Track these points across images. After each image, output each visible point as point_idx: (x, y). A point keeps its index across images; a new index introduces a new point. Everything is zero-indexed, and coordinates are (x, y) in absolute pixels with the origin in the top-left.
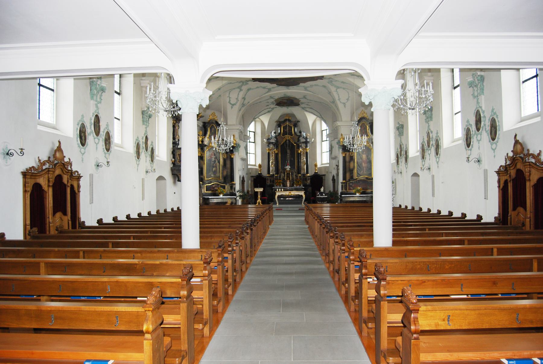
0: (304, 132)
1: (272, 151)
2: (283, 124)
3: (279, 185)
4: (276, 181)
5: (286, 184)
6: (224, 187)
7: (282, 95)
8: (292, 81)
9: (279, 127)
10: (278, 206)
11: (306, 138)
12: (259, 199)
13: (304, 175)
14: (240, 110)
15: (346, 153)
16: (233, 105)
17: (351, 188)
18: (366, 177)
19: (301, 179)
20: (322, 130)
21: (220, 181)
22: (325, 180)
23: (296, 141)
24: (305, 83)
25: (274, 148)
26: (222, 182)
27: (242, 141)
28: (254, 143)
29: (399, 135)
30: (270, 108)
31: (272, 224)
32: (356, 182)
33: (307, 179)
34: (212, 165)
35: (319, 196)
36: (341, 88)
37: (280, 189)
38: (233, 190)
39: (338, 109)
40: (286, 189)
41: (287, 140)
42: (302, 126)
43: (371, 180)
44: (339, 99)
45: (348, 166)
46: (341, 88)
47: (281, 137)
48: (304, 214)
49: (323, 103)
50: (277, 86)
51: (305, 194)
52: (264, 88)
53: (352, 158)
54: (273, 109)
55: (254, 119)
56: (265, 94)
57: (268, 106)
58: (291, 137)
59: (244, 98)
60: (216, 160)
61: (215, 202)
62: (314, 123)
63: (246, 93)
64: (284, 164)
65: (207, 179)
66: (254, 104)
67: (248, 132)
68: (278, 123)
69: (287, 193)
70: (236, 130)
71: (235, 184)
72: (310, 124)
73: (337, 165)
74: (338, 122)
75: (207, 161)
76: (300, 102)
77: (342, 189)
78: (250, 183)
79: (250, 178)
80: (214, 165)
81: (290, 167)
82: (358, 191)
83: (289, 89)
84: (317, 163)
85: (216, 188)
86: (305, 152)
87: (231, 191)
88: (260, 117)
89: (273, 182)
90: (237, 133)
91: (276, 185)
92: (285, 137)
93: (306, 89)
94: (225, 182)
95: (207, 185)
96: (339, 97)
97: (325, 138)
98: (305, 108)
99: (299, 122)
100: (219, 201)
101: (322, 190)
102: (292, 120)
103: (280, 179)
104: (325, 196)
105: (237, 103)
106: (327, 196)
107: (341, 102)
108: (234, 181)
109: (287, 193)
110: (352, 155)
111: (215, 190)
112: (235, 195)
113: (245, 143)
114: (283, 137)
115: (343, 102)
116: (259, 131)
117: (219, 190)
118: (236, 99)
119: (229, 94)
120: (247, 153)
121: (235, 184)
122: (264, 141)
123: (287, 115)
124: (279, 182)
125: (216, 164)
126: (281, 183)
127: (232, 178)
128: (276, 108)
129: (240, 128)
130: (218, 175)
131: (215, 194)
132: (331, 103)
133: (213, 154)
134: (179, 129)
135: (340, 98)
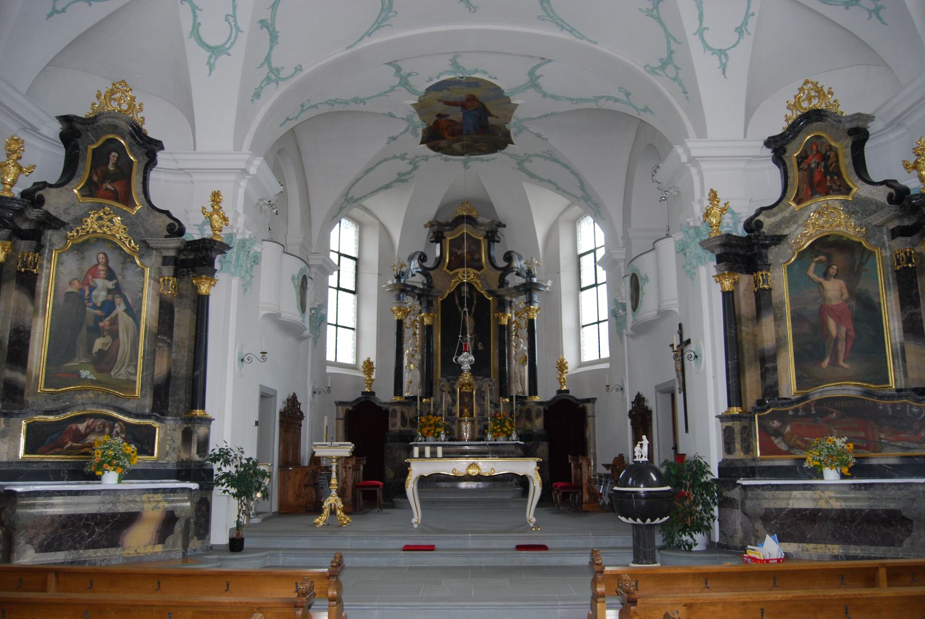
1: (413, 318)
5: (460, 431)
9: (437, 242)
11: (530, 274)
12: (334, 492)
13: (521, 399)
14: (257, 95)
16: (216, 51)
19: (511, 413)
20: (580, 251)
23: (494, 287)
25: (418, 308)
30: (403, 157)
33: (534, 413)
34: (90, 321)
37: (428, 450)
40: (460, 448)
42: (510, 240)
44: (700, 33)
47: (445, 272)
49: (609, 98)
51: (539, 471)
61: (54, 518)
62: (552, 233)
64: (452, 346)
69: (460, 466)
70: (233, 177)
71: (208, 421)
72: (540, 233)
75: (61, 300)
76: (513, 120)
77: (728, 446)
78: (326, 424)
80: (105, 323)
81: (472, 358)
82: (836, 459)
86: (524, 323)
87: (184, 456)
89: (414, 423)
94: (160, 409)
99: (504, 226)
100: (88, 506)
102: (480, 220)
103: (439, 412)
104: (661, 482)
106: (668, 488)
107: (707, 47)
108: (203, 407)
109: (460, 466)
115: (717, 47)
116: (372, 256)
121: (208, 421)
123: (465, 202)
124: (432, 422)
125: (115, 321)
126: (440, 427)
128: (427, 158)
132: (649, 76)
133: (102, 273)
135: (704, 25)
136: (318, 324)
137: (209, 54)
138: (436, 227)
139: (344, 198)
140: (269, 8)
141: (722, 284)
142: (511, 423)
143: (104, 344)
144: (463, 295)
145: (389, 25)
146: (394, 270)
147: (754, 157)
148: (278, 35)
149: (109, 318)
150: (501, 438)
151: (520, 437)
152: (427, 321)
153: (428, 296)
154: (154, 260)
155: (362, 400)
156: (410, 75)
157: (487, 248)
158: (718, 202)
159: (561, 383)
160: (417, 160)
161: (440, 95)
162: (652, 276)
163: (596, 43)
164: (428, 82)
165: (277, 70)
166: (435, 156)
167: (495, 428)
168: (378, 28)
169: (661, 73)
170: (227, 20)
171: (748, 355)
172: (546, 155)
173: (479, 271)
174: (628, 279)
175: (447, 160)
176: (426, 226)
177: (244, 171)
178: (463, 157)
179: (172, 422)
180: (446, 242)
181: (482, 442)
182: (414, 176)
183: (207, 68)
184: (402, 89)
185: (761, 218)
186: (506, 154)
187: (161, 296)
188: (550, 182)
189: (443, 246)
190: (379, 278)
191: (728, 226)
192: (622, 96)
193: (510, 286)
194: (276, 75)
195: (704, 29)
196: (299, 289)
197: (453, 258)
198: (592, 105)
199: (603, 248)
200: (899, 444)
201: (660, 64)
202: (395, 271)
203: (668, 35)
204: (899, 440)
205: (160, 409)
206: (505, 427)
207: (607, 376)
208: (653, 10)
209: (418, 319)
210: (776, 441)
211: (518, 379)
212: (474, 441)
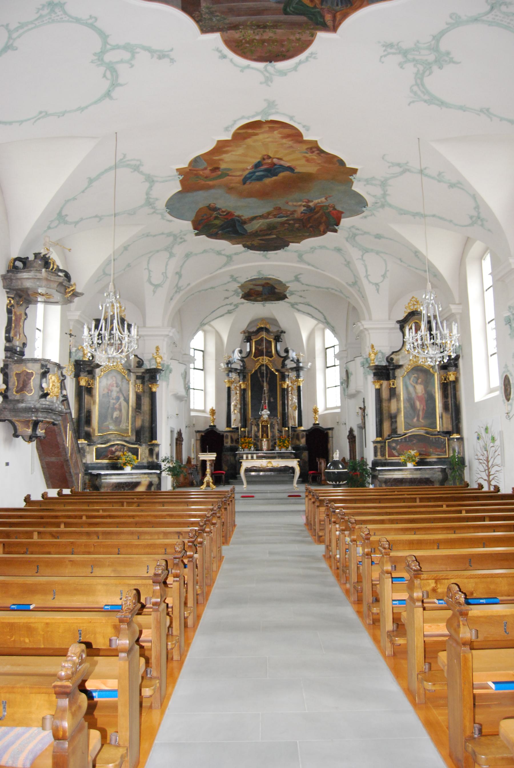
0: (293, 351)
1: (235, 385)
2: (254, 337)
3: (248, 448)
4: (243, 440)
6: (135, 452)
7: (253, 275)
8: (274, 236)
9: (247, 342)
10: (245, 489)
11: (298, 361)
13: (294, 429)
14: (171, 299)
15: (382, 381)
16: (157, 286)
17: (394, 452)
18: (426, 430)
19: (289, 436)
20: (326, 347)
21: (127, 439)
22: (332, 437)
23: (279, 367)
25: (238, 379)
26: (133, 442)
27: (177, 362)
28: (202, 370)
29: (510, 334)
30: (231, 304)
31: (233, 539)
32: (403, 440)
33: (300, 436)
34: (111, 406)
35: (330, 469)
36: (372, 250)
37: (250, 456)
38: (155, 457)
39: (363, 297)
41: (263, 365)
42: (288, 340)
43: (435, 435)
44: (367, 276)
45: (387, 408)
46: (372, 250)
47: (252, 359)
48: (303, 507)
49: (332, 289)
52: (219, 253)
53: (393, 393)
54: (237, 306)
55: (201, 326)
56: (220, 268)
57: (228, 298)
58: (270, 359)
59: (179, 274)
60: (121, 396)
62: (311, 336)
63: (183, 264)
64: (257, 407)
65: (99, 434)
66: (200, 291)
67: (192, 351)
68: (247, 334)
71: (158, 445)
72: (305, 336)
73: (360, 408)
74: (363, 322)
76: (288, 291)
77: (376, 455)
79: (195, 433)
81: (269, 412)
82: (411, 459)
83: (268, 259)
84: (318, 407)
85: (117, 453)
86: (295, 387)
87: (150, 460)
88: (212, 323)
89: (237, 441)
90: (165, 343)
91: (242, 448)
92: (259, 359)
93: (300, 257)
94: (138, 440)
95: (99, 446)
96: (367, 271)
97: (331, 361)
98: (296, 304)
99: (285, 332)
101: (336, 456)
102: (271, 330)
103: (250, 436)
106: (346, 470)
107: (370, 282)
108: (156, 439)
109: (264, 463)
110: (394, 387)
111: (117, 456)
112: (157, 467)
113: (182, 368)
114: (256, 359)
116: (212, 349)
117: (124, 458)
118: (163, 274)
119: (148, 263)
120: (187, 389)
122: (221, 367)
123: (262, 320)
125: (120, 405)
127: (153, 435)
128: (243, 303)
129: (171, 334)
130: (123, 426)
131: (115, 466)
133: (115, 385)
134: (26, 321)
135: (368, 273)
141: (375, 385)
142: (288, 441)
143: (117, 415)
144: (262, 371)
149: (118, 403)
150: (283, 449)
151: (294, 449)
152: (243, 387)
153: (243, 373)
154: (133, 377)
155: (210, 430)
159: (315, 420)
163: (324, 271)
165: (180, 287)
167: (280, 444)
171: (385, 415)
173: (271, 358)
175: (254, 304)
177: (168, 335)
178: (262, 302)
179: (144, 446)
181: (273, 452)
185: (393, 356)
186: (285, 302)
187: (136, 392)
191: (380, 358)
200: (436, 453)
203: (354, 275)
204: (437, 451)
205: (138, 440)
206: (285, 443)
207: (337, 417)
209: (238, 385)
210: (394, 452)
211: (292, 418)
212: (269, 451)
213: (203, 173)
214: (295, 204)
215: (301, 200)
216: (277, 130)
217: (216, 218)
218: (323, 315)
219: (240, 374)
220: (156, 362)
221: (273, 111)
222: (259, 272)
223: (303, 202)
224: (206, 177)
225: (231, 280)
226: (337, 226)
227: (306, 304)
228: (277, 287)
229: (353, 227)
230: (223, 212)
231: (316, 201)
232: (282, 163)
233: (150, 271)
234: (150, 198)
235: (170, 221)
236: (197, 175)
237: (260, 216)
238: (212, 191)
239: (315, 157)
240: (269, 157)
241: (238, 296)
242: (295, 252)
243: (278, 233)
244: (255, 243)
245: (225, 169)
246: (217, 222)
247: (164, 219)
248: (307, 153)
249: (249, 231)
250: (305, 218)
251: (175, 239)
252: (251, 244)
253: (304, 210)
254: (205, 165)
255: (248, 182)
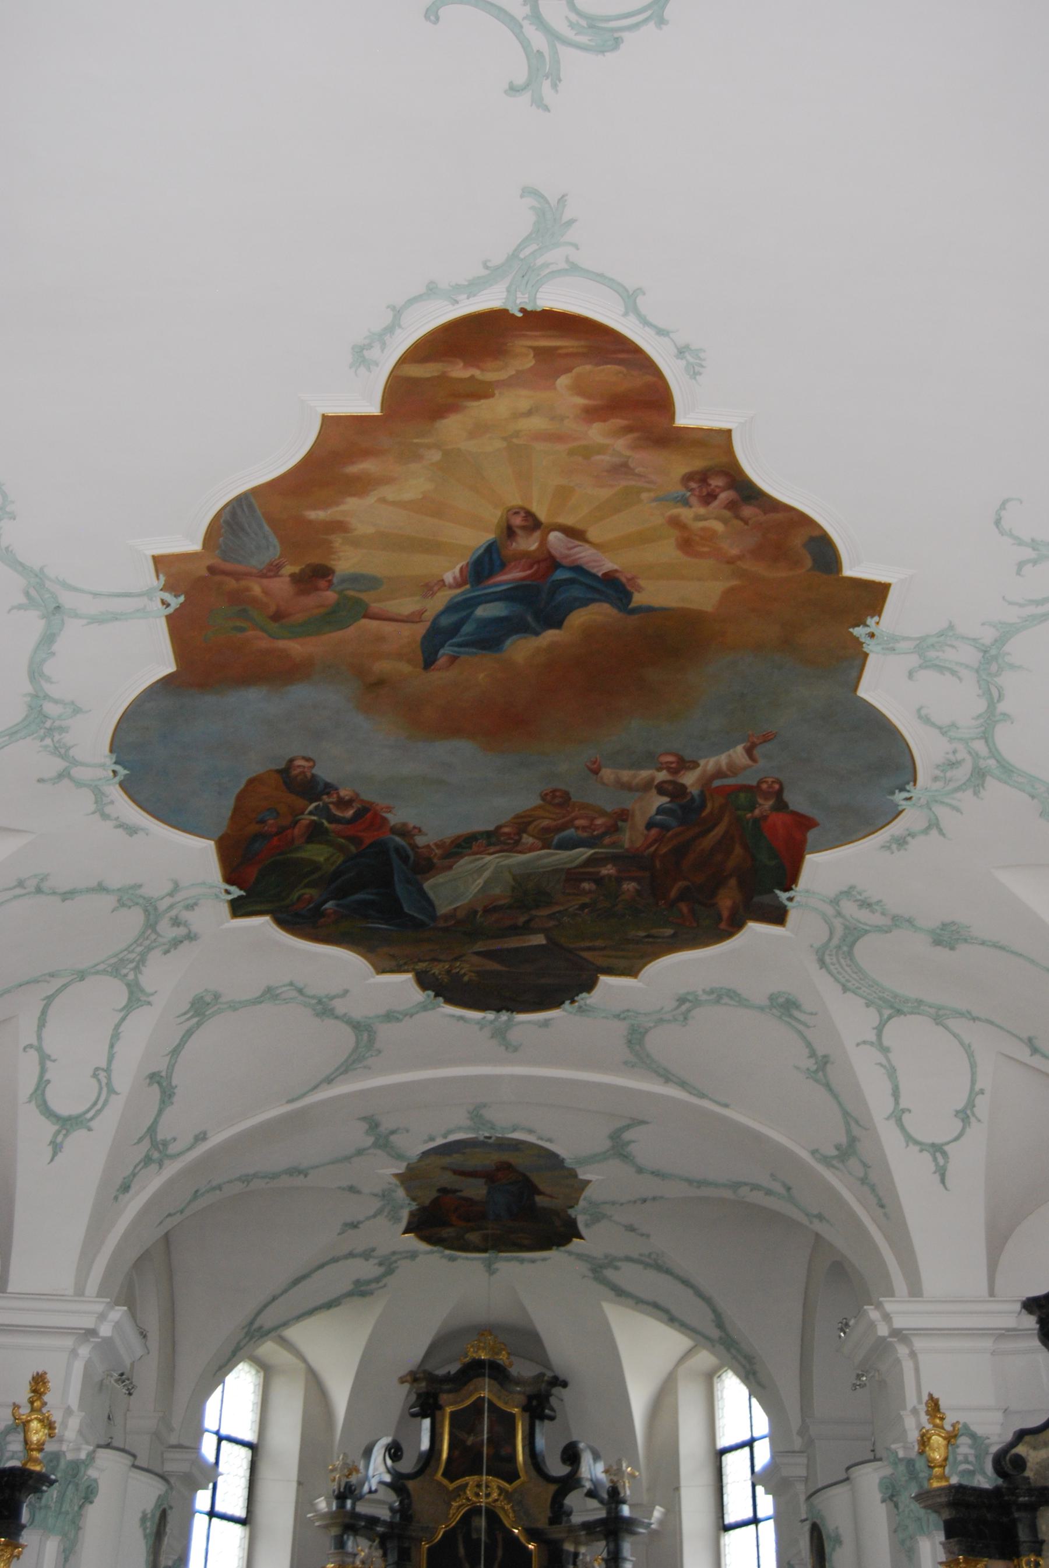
0: (597, 1457)
8: (539, 940)
9: (424, 1416)
11: (615, 1497)
14: (125, 1188)
16: (68, 1124)
20: (722, 1442)
23: (542, 1521)
24: (632, 972)
28: (243, 1522)
30: (367, 1255)
36: (918, 1006)
41: (475, 1511)
44: (898, 1116)
46: (918, 1006)
47: (440, 1484)
49: (755, 1187)
50: (418, 995)
52: (324, 1009)
54: (389, 1265)
56: (329, 1080)
57: (354, 1226)
70: (69, 1342)
76: (582, 1203)
88: (292, 1333)
96: (896, 1094)
98: (611, 1262)
99: (564, 1384)
105: (98, 1107)
107: (910, 1139)
114: (452, 1486)
119: (42, 1023)
123: (484, 1331)
128: (413, 1255)
129: (105, 1330)
132: (820, 1168)
135: (903, 1104)
136: (76, 1508)
137: (56, 1128)
138: (423, 1384)
139: (246, 1330)
140: (167, 1055)
144: (475, 1536)
145: (365, 1067)
146: (334, 1480)
147: (1008, 1330)
148: (176, 1091)
156: (393, 1132)
157: (527, 1432)
158: (942, 1419)
160: (394, 1258)
161: (447, 1160)
162: (847, 1537)
163: (726, 1106)
164: (426, 1142)
165: (165, 1144)
166: (431, 1252)
168: (346, 1072)
169: (840, 1165)
170: (95, 1075)
172: (647, 1260)
174: (807, 1526)
175: (452, 1259)
176: (402, 1380)
177: (92, 1332)
180: (443, 1416)
182: (385, 1286)
183: (49, 1151)
184: (379, 1152)
185: (1021, 1450)
186: (570, 1253)
188: (656, 1306)
189: (438, 1426)
190: (298, 1491)
191: (967, 1461)
192: (777, 1187)
193: (577, 1519)
194: (160, 1152)
195: (903, 1111)
196: (151, 1542)
197: (457, 1453)
198: (728, 1194)
199: (767, 1440)
201: (835, 1153)
202: (336, 1483)
203: (846, 1114)
208: (816, 1071)
213: (266, 592)
214: (626, 775)
215: (650, 759)
216: (569, 370)
217: (315, 833)
218: (715, 1311)
219: (389, 1545)
220: (26, 1442)
221: (556, 257)
222: (476, 1115)
223: (659, 769)
224: (277, 617)
225: (370, 1140)
226: (788, 889)
227: (647, 1265)
228: (542, 1187)
229: (848, 892)
230: (343, 803)
231: (710, 764)
232: (584, 554)
233: (44, 1059)
234: (46, 697)
235: (132, 830)
236: (239, 600)
237: (488, 834)
238: (300, 693)
239: (718, 527)
240: (533, 523)
241: (395, 1219)
242: (617, 1016)
243: (551, 923)
244: (467, 968)
245: (355, 579)
246: (318, 853)
247: (105, 816)
248: (685, 503)
249: (443, 908)
250: (664, 850)
251: (151, 925)
252: (448, 972)
253: (660, 811)
254: (274, 550)
255: (446, 651)
